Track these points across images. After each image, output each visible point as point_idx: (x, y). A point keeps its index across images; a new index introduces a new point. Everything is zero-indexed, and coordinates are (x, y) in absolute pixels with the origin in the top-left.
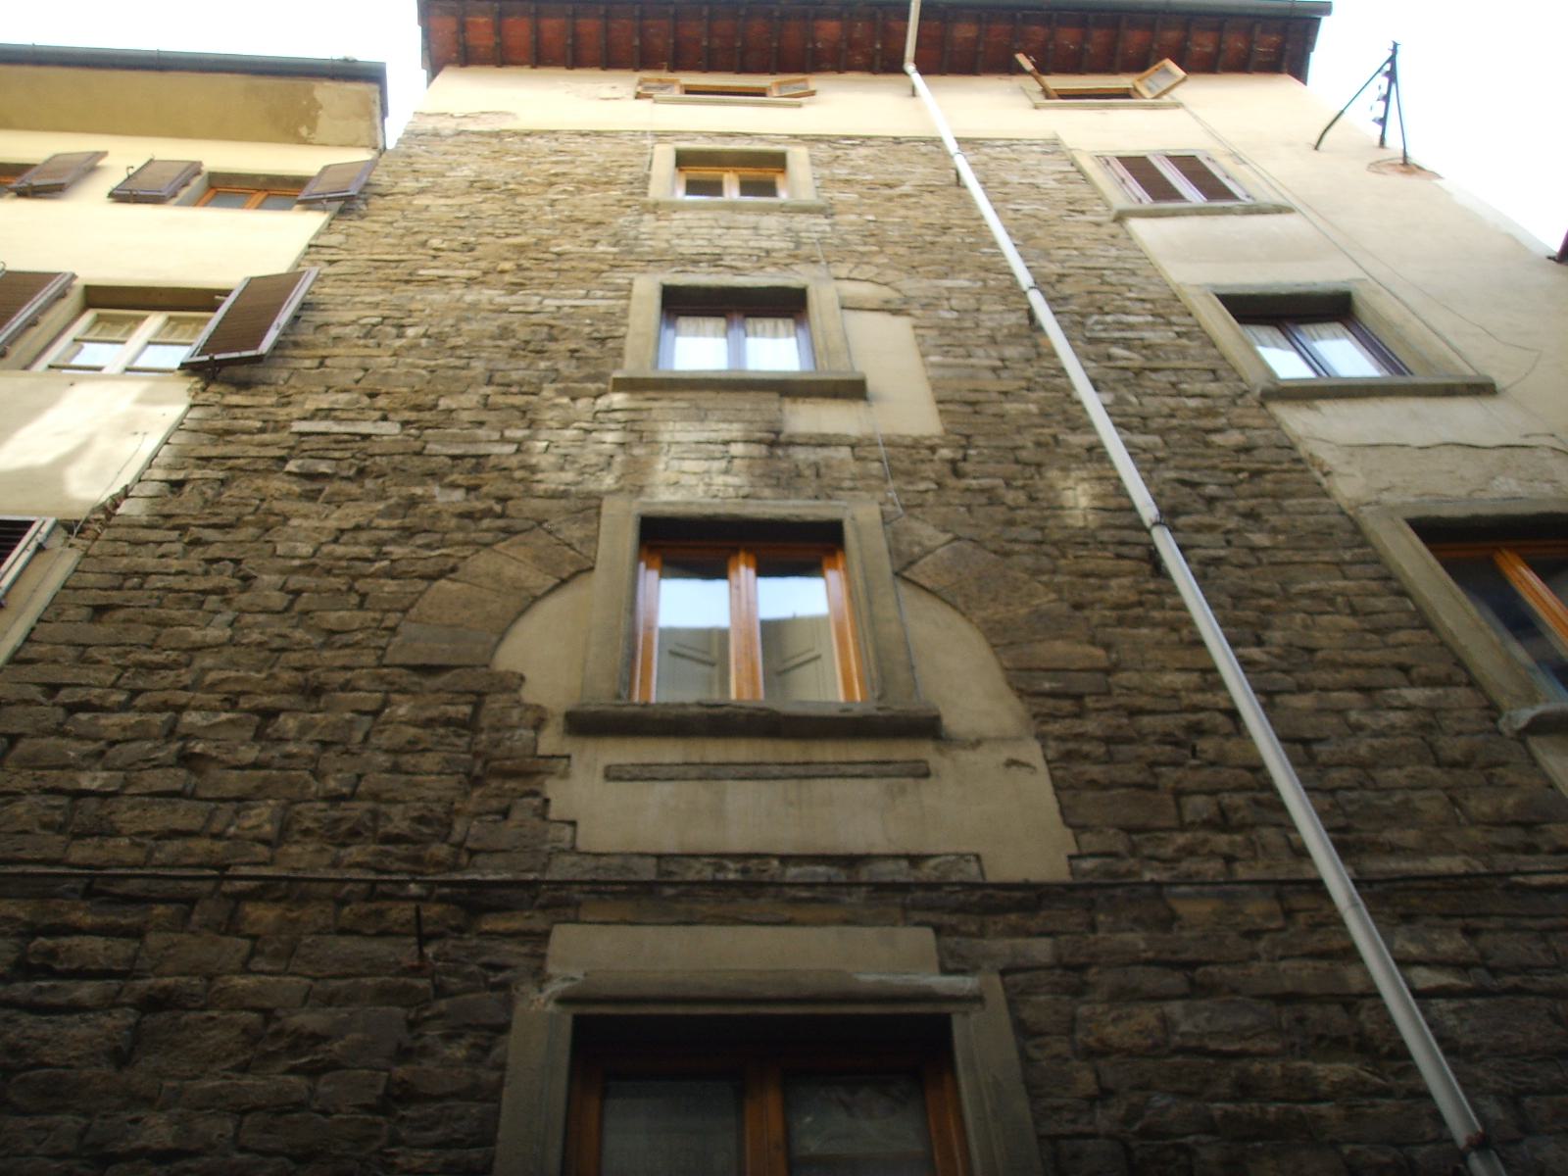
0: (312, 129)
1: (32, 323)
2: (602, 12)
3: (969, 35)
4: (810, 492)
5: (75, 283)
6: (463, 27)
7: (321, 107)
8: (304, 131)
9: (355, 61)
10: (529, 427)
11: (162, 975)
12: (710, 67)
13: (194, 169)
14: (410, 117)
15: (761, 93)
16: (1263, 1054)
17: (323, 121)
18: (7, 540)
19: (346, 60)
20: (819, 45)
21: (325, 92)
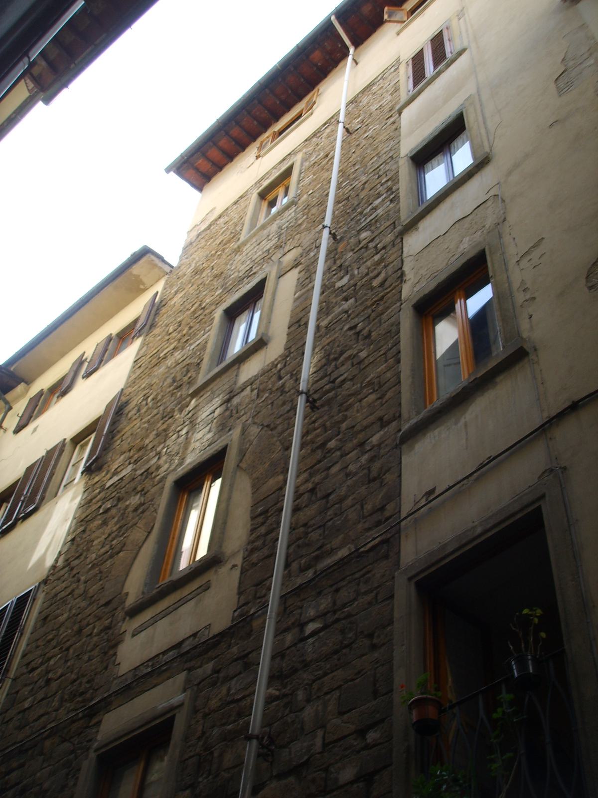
0: (143, 284)
1: (52, 474)
2: (234, 124)
3: (370, 8)
4: (155, 514)
5: (67, 441)
6: (197, 169)
7: (139, 276)
8: (142, 287)
9: (135, 253)
10: (347, 273)
11: (333, 551)
12: (277, 118)
13: (110, 339)
14: (186, 236)
15: (299, 116)
16: (333, 719)
17: (145, 280)
18: (18, 617)
19: (132, 255)
20: (319, 64)
21: (136, 270)
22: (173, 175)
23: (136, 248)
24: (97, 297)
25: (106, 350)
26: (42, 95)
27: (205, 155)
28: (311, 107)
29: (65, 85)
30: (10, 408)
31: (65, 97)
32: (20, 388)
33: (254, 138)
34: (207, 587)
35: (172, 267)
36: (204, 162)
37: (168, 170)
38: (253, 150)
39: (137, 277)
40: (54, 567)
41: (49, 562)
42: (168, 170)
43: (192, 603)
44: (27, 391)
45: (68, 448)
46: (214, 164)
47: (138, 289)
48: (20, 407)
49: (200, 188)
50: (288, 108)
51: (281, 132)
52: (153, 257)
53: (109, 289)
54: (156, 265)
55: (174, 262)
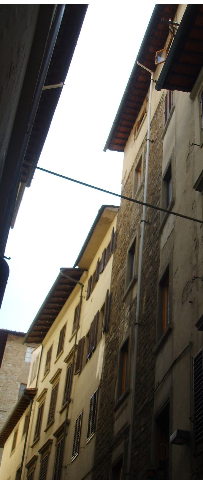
6: (117, 144)
13: (105, 251)
21: (104, 215)
22: (108, 151)
23: (99, 207)
24: (89, 244)
25: (105, 258)
26: (25, 184)
27: (116, 137)
28: (145, 112)
29: (32, 178)
30: (83, 286)
31: (33, 181)
32: (84, 274)
33: (132, 128)
34: (126, 405)
35: (118, 207)
36: (118, 140)
37: (105, 150)
38: (132, 137)
39: (106, 218)
40: (101, 380)
41: (100, 378)
42: (105, 150)
43: (124, 411)
44: (87, 274)
45: (101, 315)
46: (123, 139)
47: (109, 222)
48: (86, 284)
49: (122, 151)
50: (139, 110)
51: (141, 120)
52: (108, 208)
53: (97, 226)
54: (111, 211)
55: (119, 205)
